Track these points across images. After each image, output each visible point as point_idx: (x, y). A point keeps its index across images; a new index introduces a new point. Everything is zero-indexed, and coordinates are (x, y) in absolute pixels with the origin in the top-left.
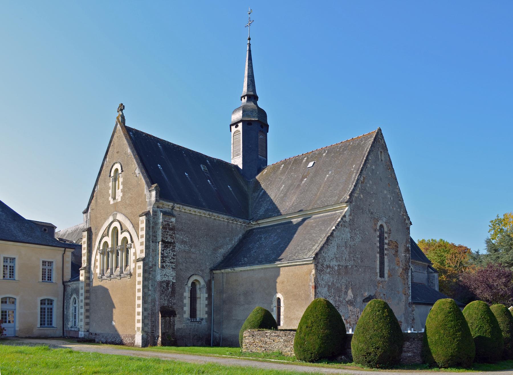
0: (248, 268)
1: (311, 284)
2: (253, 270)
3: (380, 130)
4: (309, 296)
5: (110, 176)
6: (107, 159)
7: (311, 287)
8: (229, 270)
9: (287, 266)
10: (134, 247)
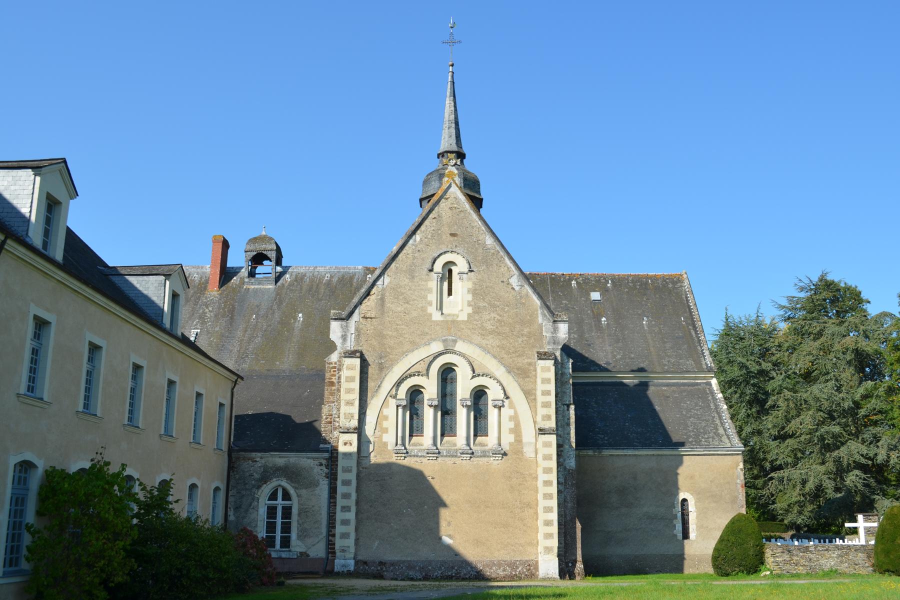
0: (630, 452)
1: (738, 481)
2: (635, 455)
3: (48, 193)
4: (737, 497)
5: (431, 270)
6: (418, 237)
7: (739, 486)
8: (590, 453)
9: (732, 455)
10: (512, 406)
